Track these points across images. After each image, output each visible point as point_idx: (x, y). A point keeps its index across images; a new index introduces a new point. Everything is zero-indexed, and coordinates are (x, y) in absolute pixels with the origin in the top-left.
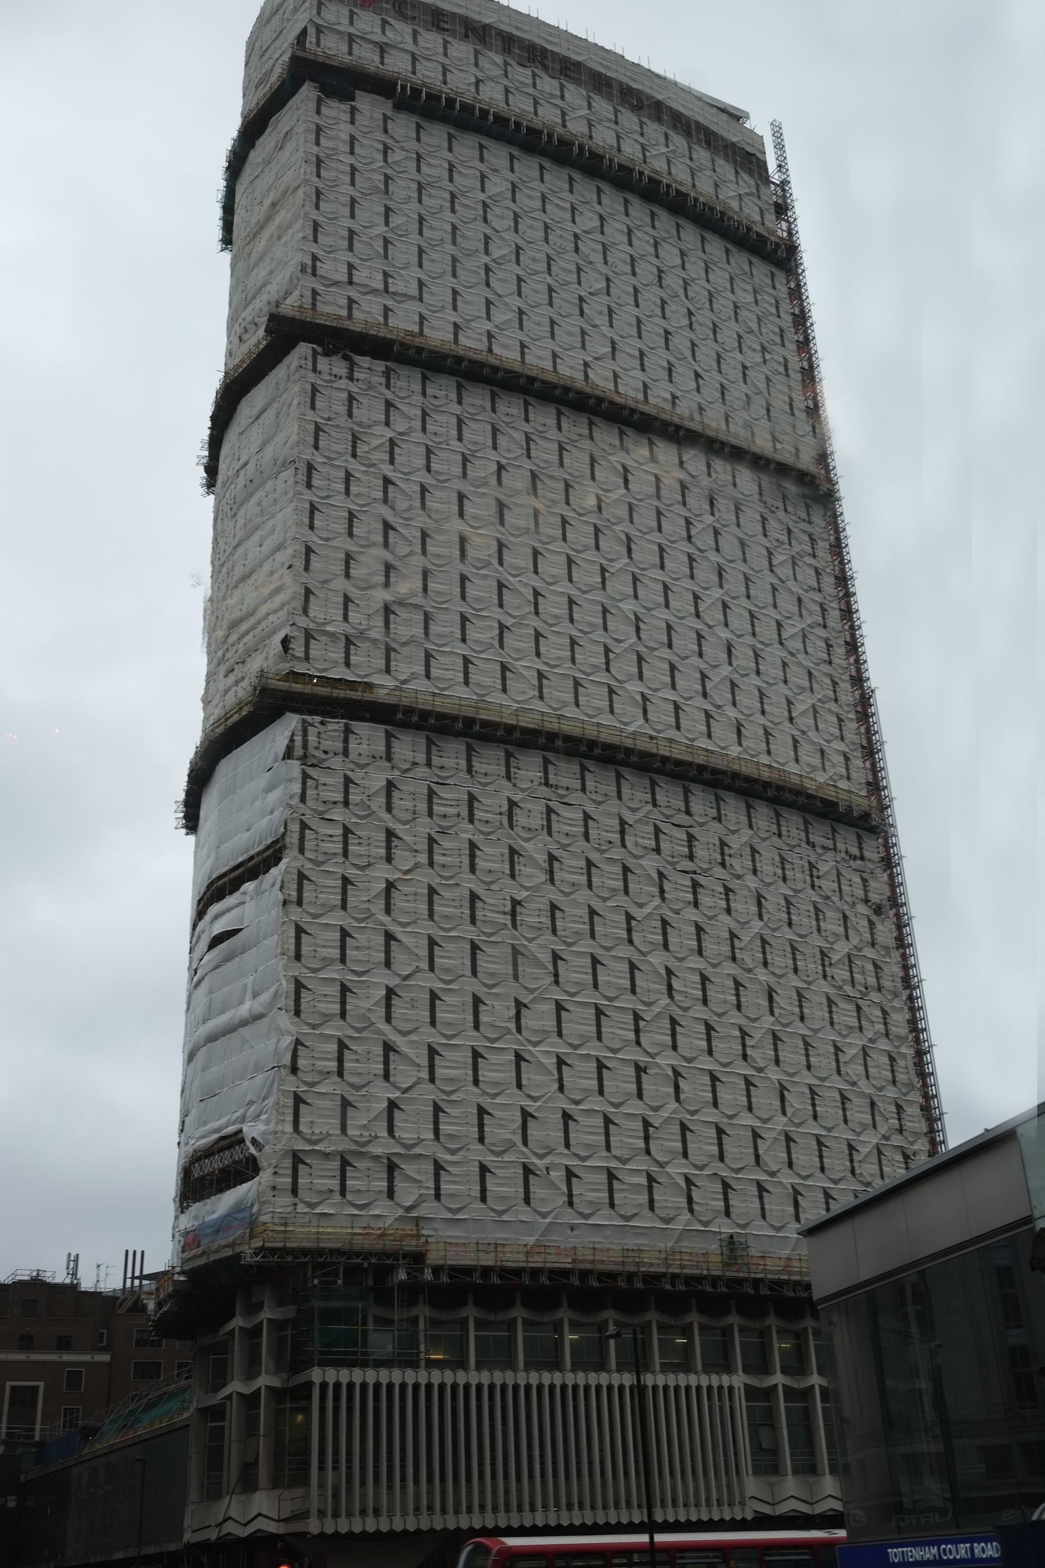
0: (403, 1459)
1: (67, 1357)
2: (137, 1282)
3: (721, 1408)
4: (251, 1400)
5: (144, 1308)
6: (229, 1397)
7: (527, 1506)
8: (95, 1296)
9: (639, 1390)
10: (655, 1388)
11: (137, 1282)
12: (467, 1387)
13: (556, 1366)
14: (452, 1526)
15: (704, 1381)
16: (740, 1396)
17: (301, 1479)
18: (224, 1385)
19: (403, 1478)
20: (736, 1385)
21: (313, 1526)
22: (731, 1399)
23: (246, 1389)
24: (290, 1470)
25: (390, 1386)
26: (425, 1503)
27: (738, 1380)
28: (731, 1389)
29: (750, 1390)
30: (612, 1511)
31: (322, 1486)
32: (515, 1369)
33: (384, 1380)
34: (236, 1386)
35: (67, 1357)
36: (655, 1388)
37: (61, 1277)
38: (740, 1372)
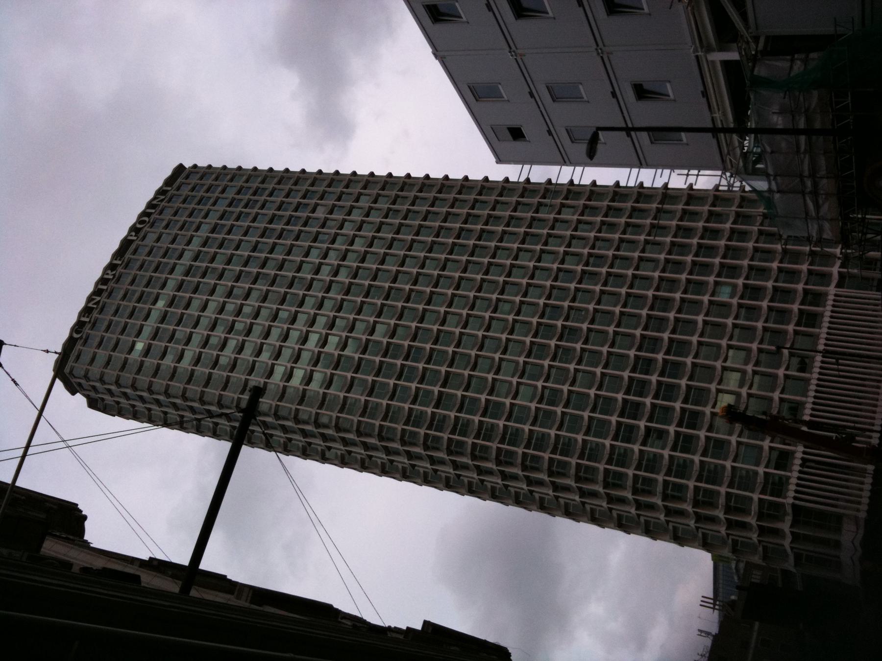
0: (855, 397)
1: (753, 645)
2: (717, 607)
3: (845, 302)
4: (795, 537)
5: (733, 601)
6: (792, 548)
7: (872, 415)
8: (722, 625)
9: (825, 353)
10: (826, 345)
11: (717, 607)
12: (799, 478)
13: (807, 381)
14: (870, 487)
15: (816, 376)
16: (841, 291)
17: (839, 518)
18: (785, 551)
19: (847, 487)
20: (834, 292)
21: (863, 515)
22: (840, 301)
23: (789, 538)
24: (835, 522)
25: (817, 385)
26: (858, 485)
27: (832, 290)
28: (836, 295)
29: (839, 285)
30: (861, 507)
31: (845, 508)
32: (805, 403)
33: (827, 325)
34: (787, 543)
35: (753, 645)
36: (826, 345)
37: (708, 642)
38: (829, 289)
